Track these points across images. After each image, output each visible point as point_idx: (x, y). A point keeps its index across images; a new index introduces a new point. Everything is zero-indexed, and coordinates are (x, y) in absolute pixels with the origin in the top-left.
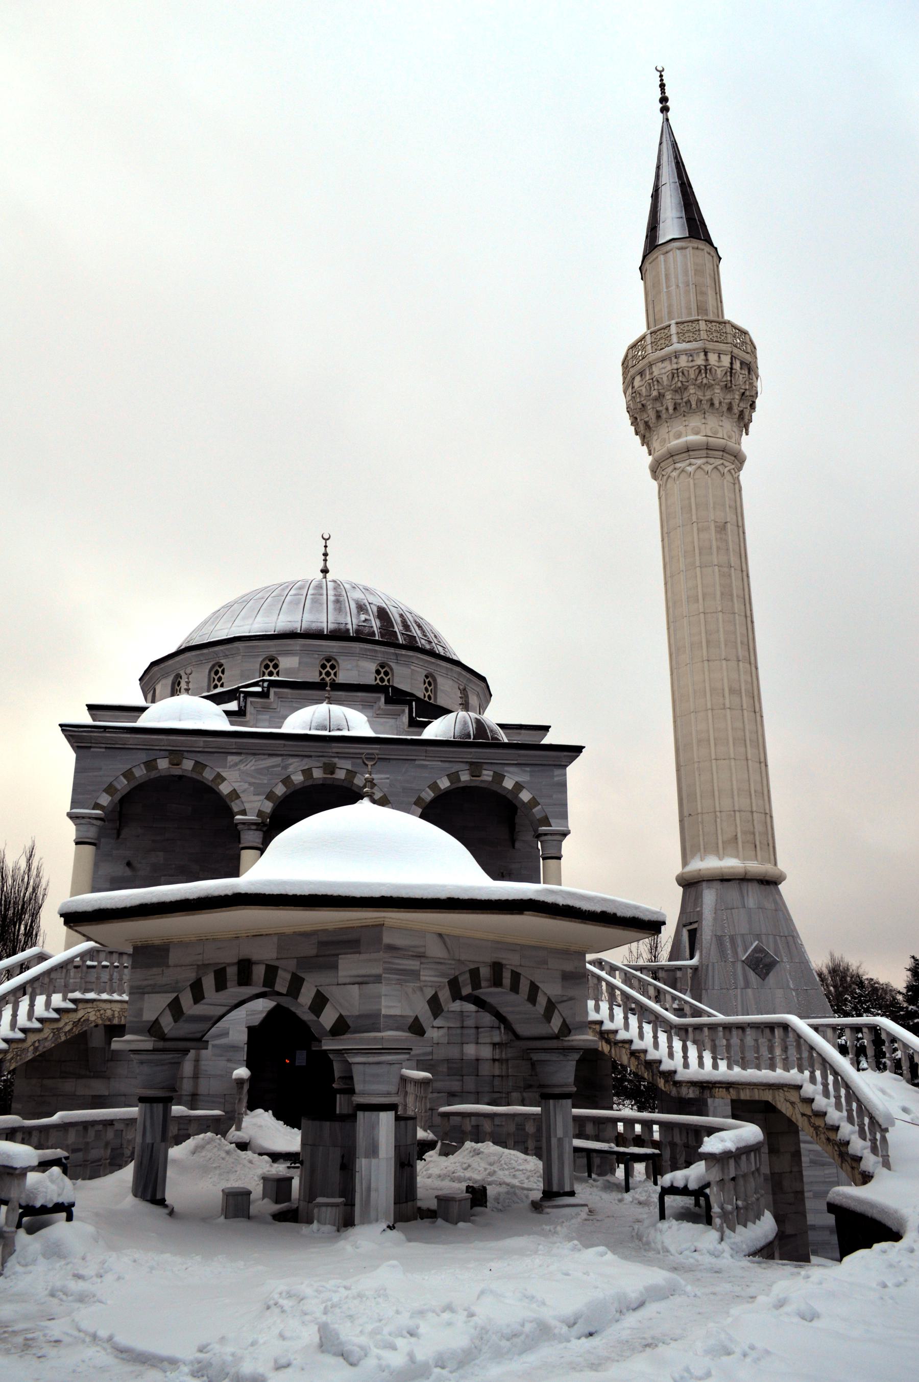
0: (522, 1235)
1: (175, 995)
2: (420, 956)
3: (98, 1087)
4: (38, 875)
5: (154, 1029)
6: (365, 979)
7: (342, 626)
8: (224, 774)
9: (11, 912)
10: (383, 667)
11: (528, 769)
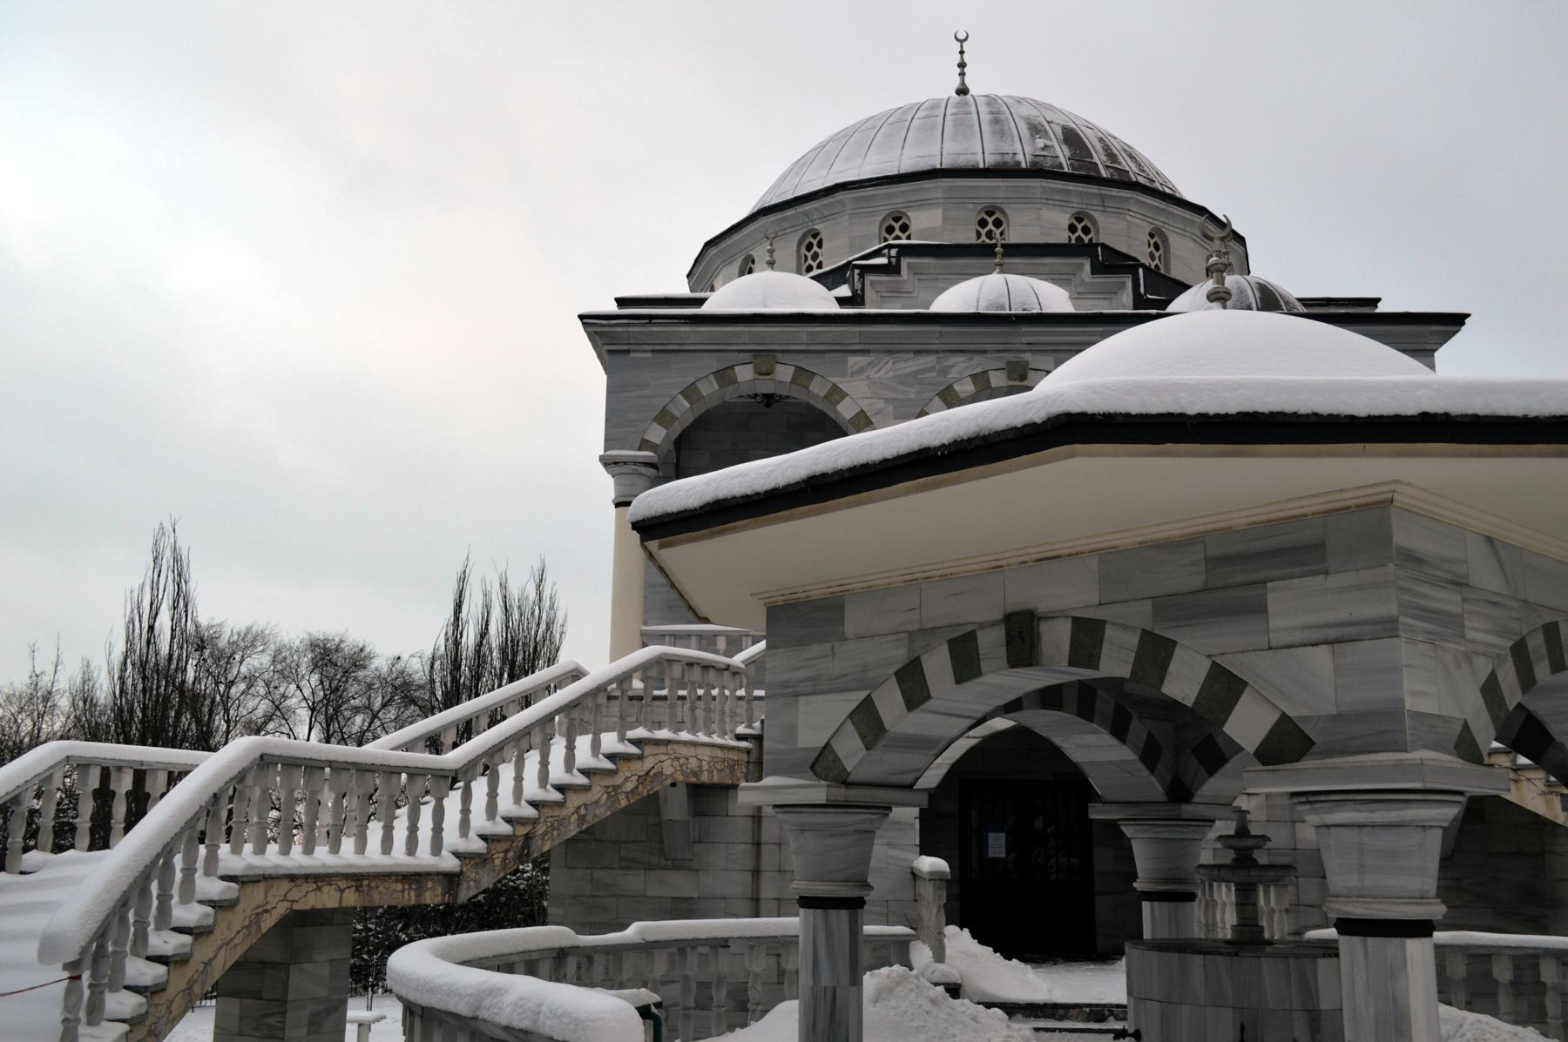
1: (862, 695)
2: (1459, 584)
3: (680, 884)
4: (551, 607)
5: (823, 763)
6: (1347, 631)
7: (1008, 158)
8: (843, 387)
9: (520, 658)
10: (1080, 220)
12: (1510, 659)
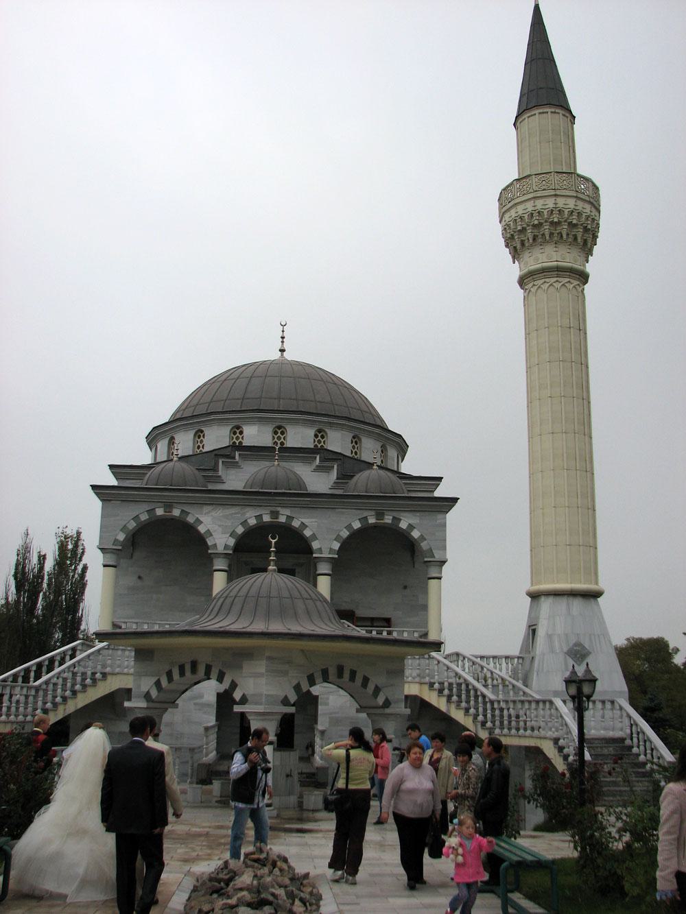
8: (201, 519)
10: (320, 432)
11: (418, 514)
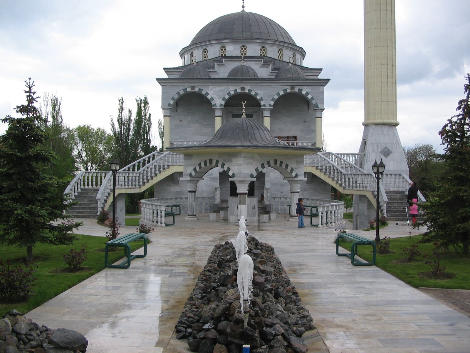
0: (393, 239)
1: (194, 167)
8: (208, 92)
12: (125, 208)
